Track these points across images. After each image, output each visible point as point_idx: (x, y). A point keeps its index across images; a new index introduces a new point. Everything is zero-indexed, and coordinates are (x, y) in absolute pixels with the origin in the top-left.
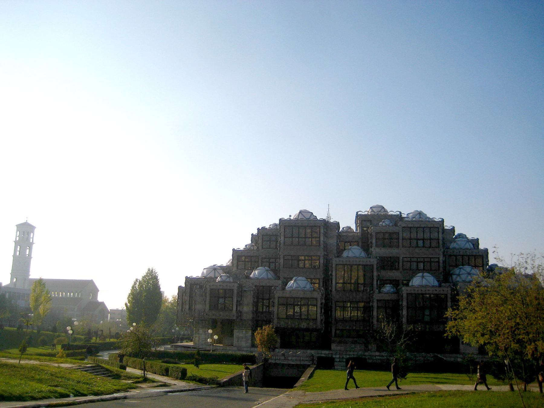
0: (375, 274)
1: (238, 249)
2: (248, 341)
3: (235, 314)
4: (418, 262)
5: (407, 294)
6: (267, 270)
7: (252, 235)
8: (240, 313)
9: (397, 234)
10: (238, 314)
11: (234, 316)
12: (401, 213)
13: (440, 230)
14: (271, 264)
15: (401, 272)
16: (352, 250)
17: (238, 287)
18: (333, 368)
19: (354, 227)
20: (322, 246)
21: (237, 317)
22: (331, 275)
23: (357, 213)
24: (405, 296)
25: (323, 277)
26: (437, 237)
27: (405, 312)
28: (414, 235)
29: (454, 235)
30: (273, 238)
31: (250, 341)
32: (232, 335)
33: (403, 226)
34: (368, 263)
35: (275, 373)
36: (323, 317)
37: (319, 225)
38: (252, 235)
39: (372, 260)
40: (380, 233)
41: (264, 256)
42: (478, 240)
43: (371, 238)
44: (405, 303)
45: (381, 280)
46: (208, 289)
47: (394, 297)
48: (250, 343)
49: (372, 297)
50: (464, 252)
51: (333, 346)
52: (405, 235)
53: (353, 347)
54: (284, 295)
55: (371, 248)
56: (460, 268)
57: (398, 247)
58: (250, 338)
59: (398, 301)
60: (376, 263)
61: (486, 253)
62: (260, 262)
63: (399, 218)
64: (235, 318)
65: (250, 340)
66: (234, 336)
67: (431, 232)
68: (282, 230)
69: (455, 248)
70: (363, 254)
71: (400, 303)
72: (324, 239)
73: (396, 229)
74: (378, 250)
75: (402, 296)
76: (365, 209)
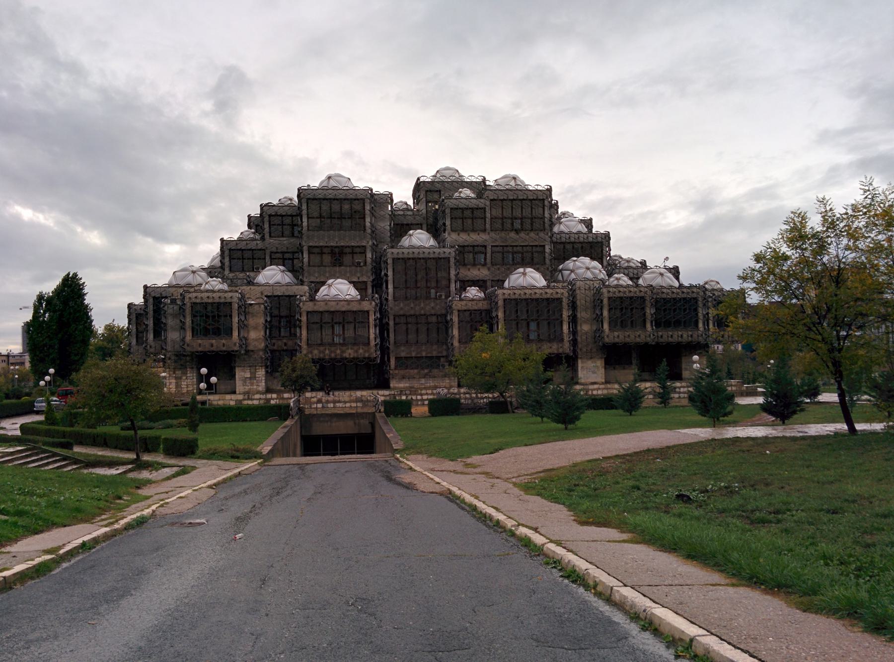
0: (453, 272)
1: (229, 239)
2: (260, 384)
3: (238, 341)
4: (513, 253)
5: (505, 300)
6: (283, 271)
7: (249, 217)
8: (244, 340)
9: (483, 211)
10: (242, 341)
11: (235, 344)
12: (484, 178)
13: (546, 203)
14: (291, 261)
15: (489, 269)
16: (197, 276)
17: (240, 300)
18: (409, 415)
19: (410, 202)
20: (369, 231)
21: (241, 346)
22: (386, 275)
23: (418, 179)
24: (501, 303)
25: (371, 279)
26: (312, 256)
27: (456, 332)
28: (507, 213)
29: (557, 213)
30: (288, 221)
31: (264, 384)
32: (233, 376)
33: (492, 198)
34: (442, 256)
35: (319, 429)
36: (378, 340)
37: (361, 197)
38: (249, 217)
39: (447, 250)
40: (457, 209)
41: (274, 250)
42: (591, 220)
43: (444, 218)
44: (501, 315)
45: (461, 281)
46: (189, 305)
47: (483, 306)
48: (264, 387)
49: (451, 307)
50: (585, 238)
51: (393, 384)
52: (494, 213)
53: (423, 382)
54: (316, 308)
55: (444, 232)
56: (574, 261)
57: (484, 231)
58: (264, 378)
59: (489, 312)
60: (453, 254)
61: (607, 238)
62: (268, 258)
63: (480, 187)
64: (236, 348)
65: (264, 381)
66: (237, 376)
67: (533, 206)
68: (304, 207)
69: (562, 232)
70: (432, 242)
71: (494, 315)
72: (371, 220)
73: (481, 203)
74: (454, 236)
75: (497, 303)
76: (428, 173)
